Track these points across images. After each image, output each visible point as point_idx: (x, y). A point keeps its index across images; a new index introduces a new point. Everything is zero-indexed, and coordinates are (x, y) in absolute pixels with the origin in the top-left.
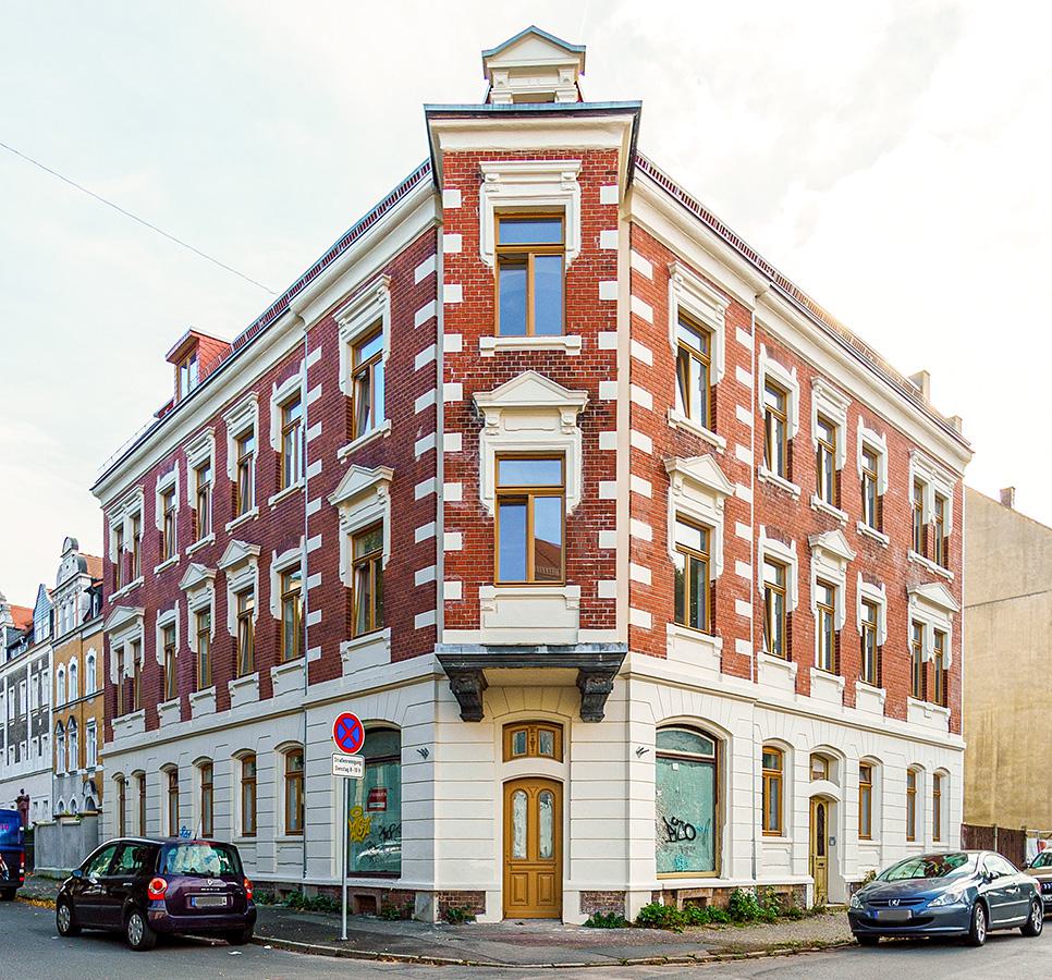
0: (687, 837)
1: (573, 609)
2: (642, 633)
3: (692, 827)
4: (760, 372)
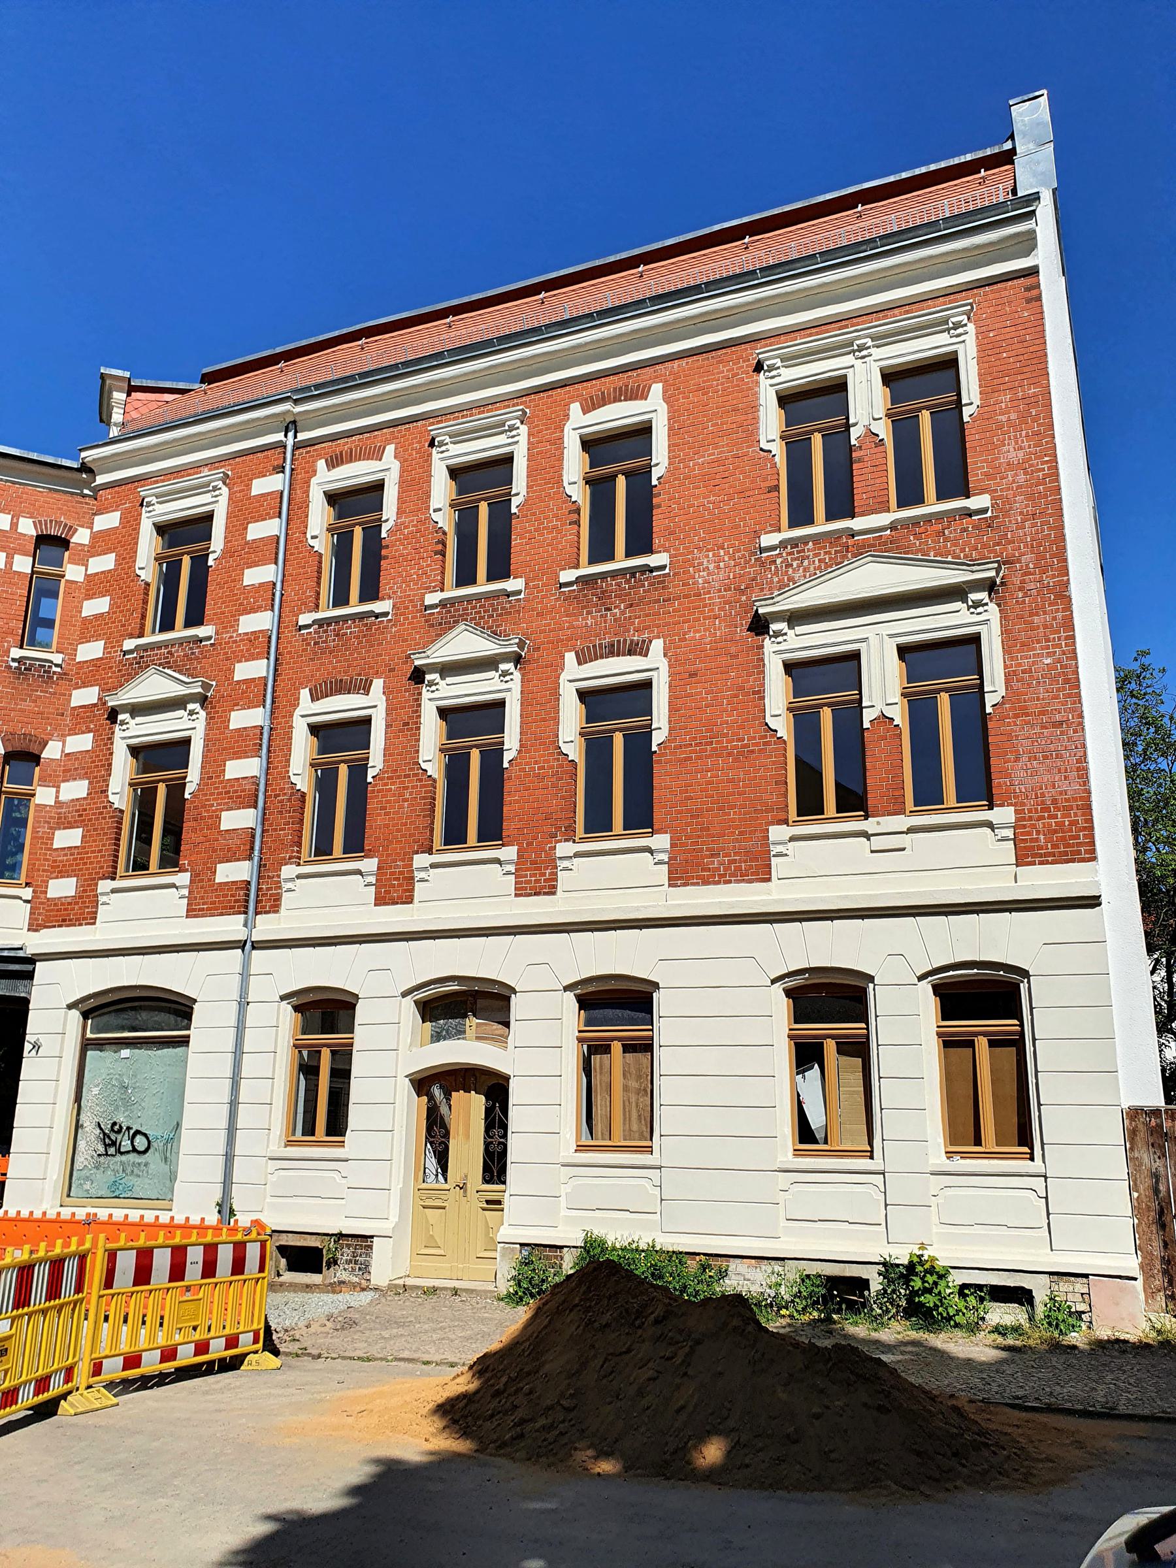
0: (134, 1150)
1: (508, 873)
2: (63, 904)
3: (145, 1135)
4: (213, 505)
